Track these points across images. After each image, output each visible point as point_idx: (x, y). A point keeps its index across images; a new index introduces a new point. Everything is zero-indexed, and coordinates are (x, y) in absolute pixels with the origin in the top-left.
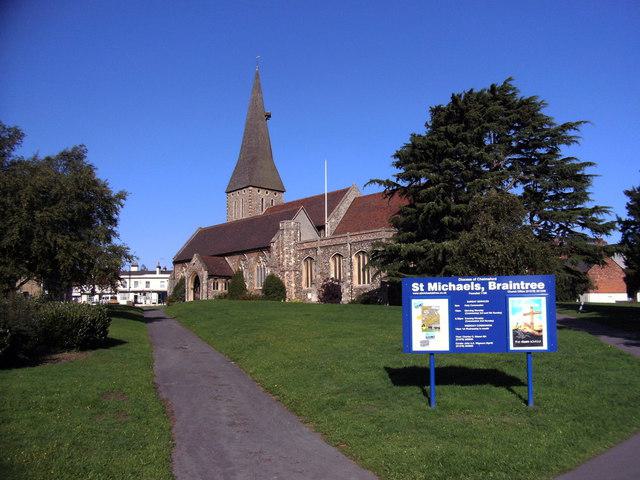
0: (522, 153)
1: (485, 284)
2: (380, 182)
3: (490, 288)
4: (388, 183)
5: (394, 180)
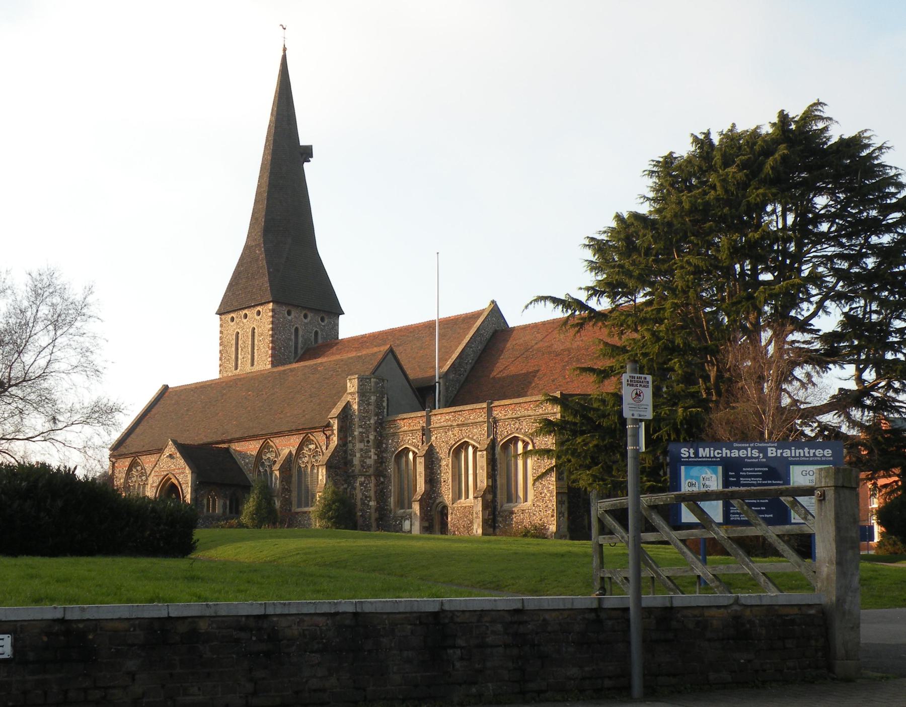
0: (842, 245)
1: (763, 450)
2: (556, 301)
3: (770, 455)
4: (566, 303)
5: (582, 296)
